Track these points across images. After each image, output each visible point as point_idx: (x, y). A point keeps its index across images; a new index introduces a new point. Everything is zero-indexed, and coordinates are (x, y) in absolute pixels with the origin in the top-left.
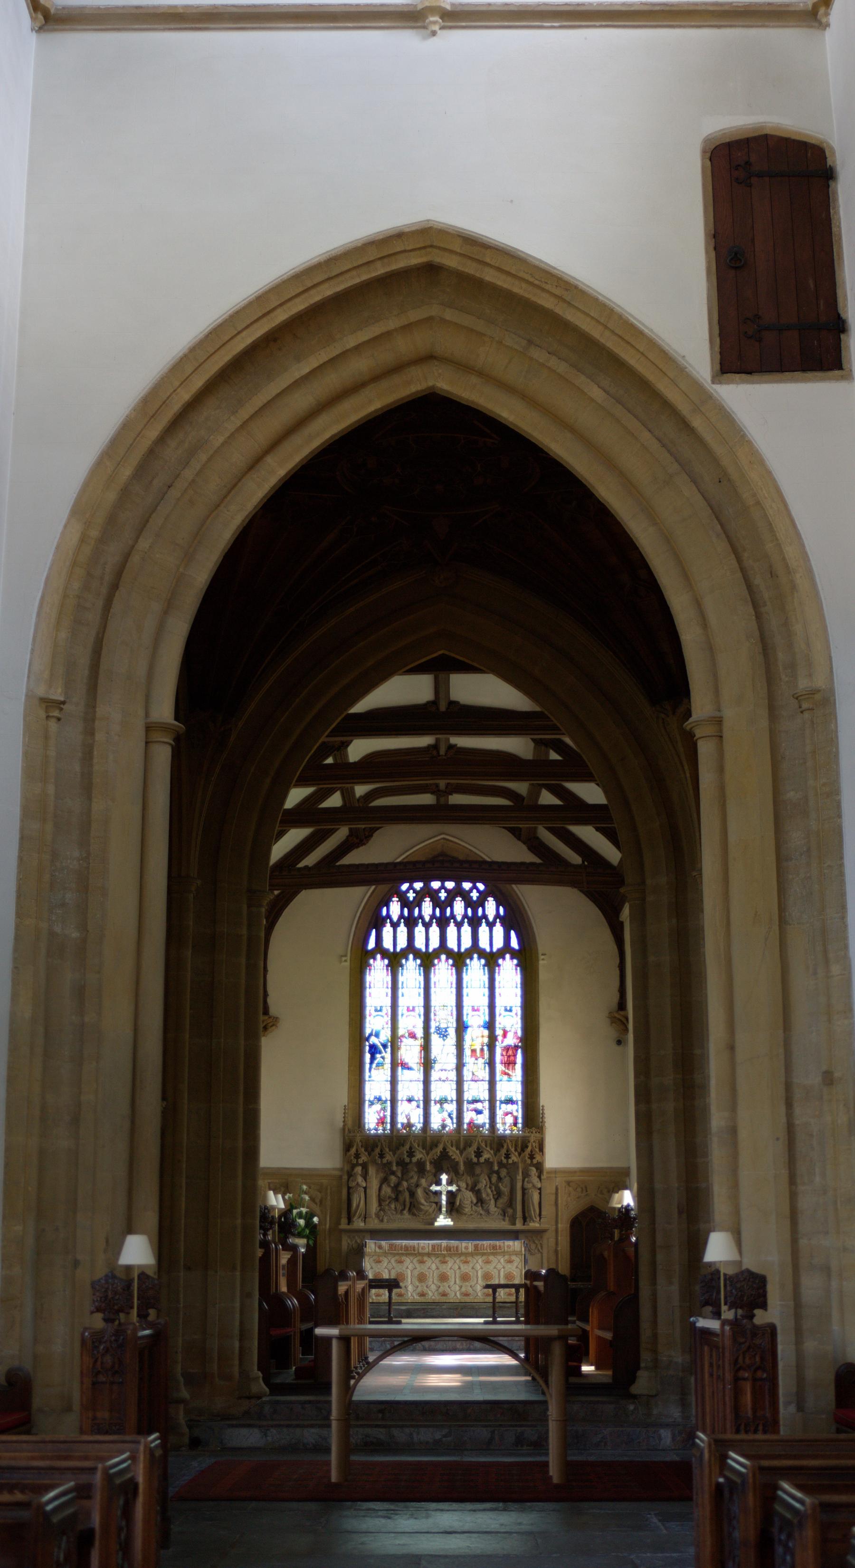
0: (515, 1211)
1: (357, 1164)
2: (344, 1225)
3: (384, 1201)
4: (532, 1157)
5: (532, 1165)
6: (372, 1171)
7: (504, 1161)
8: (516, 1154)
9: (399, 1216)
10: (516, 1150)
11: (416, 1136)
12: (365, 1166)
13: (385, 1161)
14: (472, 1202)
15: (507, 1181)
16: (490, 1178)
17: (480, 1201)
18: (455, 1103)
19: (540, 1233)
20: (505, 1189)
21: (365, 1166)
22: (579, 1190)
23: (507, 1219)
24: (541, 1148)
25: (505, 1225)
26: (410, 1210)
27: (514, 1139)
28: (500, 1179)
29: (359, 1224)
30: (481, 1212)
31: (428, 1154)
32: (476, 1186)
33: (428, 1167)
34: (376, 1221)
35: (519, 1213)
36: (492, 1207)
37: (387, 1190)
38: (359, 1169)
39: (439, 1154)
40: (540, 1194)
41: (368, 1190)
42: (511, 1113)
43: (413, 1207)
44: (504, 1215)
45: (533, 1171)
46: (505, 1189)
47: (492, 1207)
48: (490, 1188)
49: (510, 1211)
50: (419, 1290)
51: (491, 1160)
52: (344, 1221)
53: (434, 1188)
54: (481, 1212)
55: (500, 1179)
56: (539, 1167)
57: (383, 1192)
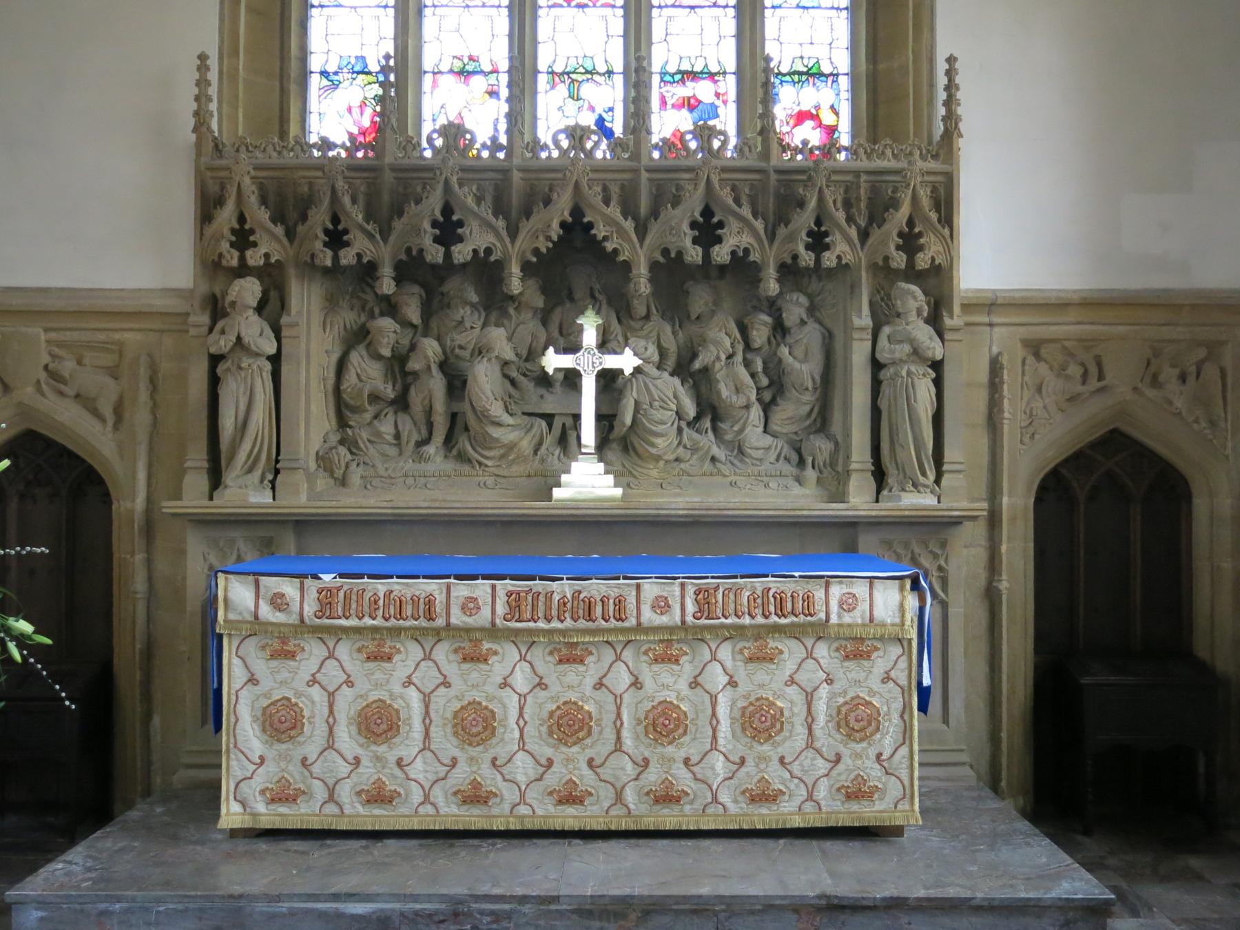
0: (841, 449)
1: (243, 270)
2: (193, 496)
3: (355, 410)
4: (910, 243)
5: (912, 274)
6: (305, 299)
7: (807, 258)
8: (853, 232)
9: (409, 465)
10: (850, 219)
11: (473, 171)
12: (272, 276)
13: (348, 257)
14: (679, 415)
15: (810, 336)
16: (743, 329)
17: (710, 411)
18: (619, 80)
19: (935, 528)
20: (803, 366)
21: (272, 276)
22: (1075, 370)
23: (811, 474)
24: (945, 204)
25: (801, 498)
26: (449, 441)
27: (849, 181)
28: (780, 330)
29: (247, 494)
30: (715, 451)
31: (513, 232)
32: (694, 356)
33: (515, 284)
34: (323, 482)
35: (860, 454)
36: (754, 435)
37: (367, 373)
38: (249, 290)
39: (555, 232)
40: (938, 383)
41: (285, 369)
42: (815, 118)
43: (459, 432)
44: (801, 463)
45: (913, 298)
46: (803, 366)
47: (754, 435)
48: (747, 364)
49: (821, 447)
50: (461, 776)
51: (754, 257)
52: (196, 482)
53: (553, 361)
54: (715, 451)
55: (780, 330)
56: (936, 282)
57: (350, 379)
